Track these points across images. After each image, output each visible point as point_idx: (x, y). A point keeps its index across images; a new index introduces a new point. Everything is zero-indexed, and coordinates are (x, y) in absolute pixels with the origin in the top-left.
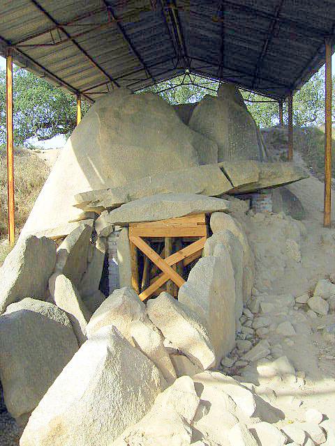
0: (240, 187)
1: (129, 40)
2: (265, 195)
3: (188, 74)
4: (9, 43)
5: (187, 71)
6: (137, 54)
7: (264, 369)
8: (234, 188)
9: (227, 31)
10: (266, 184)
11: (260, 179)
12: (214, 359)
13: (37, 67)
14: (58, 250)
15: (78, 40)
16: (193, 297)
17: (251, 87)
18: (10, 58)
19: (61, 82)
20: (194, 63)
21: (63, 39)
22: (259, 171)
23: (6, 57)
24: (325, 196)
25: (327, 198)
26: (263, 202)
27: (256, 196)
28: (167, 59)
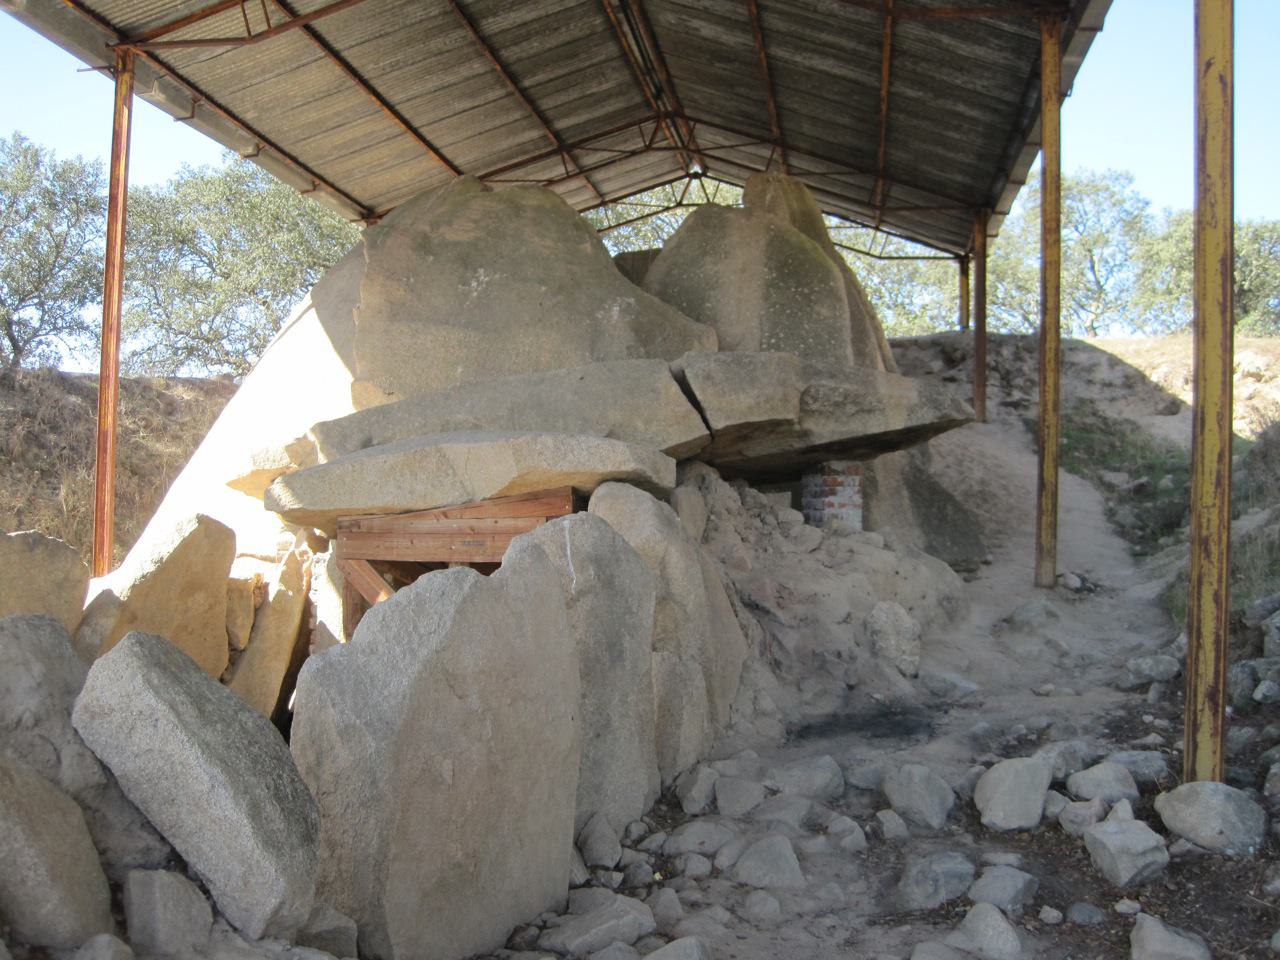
0: (745, 432)
1: (494, 52)
2: (840, 479)
3: (696, 176)
4: (125, 35)
5: (696, 168)
6: (528, 98)
7: (32, 852)
8: (713, 435)
9: (773, 21)
10: (825, 431)
11: (804, 410)
12: (282, 883)
13: (231, 124)
14: (95, 587)
15: (319, 24)
16: (342, 693)
17: (878, 211)
18: (126, 77)
19: (317, 180)
20: (706, 137)
21: (274, 22)
22: (802, 386)
23: (114, 72)
24: (1040, 496)
25: (1047, 503)
26: (831, 499)
27: (814, 482)
28: (991, 341)
